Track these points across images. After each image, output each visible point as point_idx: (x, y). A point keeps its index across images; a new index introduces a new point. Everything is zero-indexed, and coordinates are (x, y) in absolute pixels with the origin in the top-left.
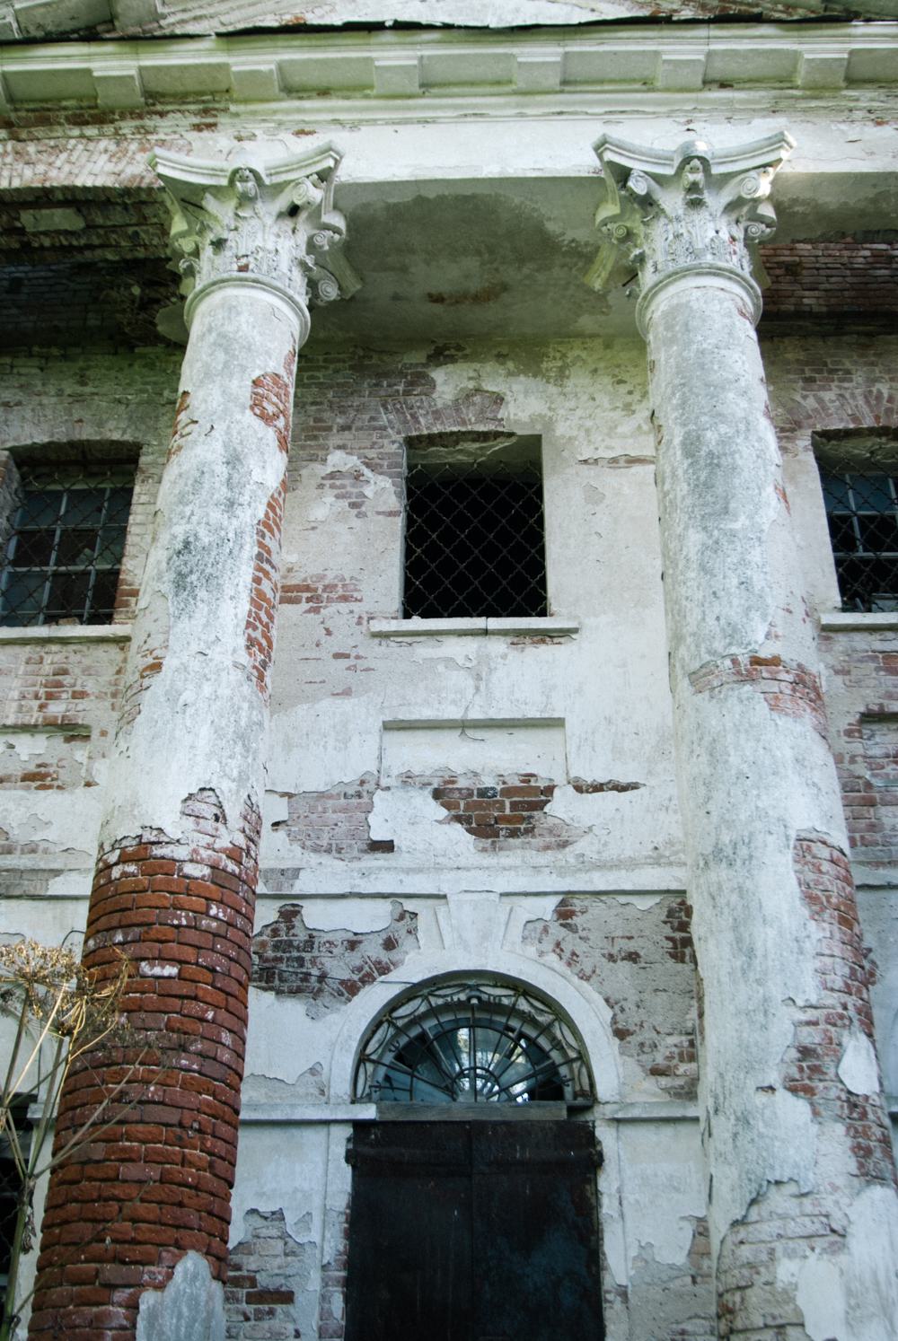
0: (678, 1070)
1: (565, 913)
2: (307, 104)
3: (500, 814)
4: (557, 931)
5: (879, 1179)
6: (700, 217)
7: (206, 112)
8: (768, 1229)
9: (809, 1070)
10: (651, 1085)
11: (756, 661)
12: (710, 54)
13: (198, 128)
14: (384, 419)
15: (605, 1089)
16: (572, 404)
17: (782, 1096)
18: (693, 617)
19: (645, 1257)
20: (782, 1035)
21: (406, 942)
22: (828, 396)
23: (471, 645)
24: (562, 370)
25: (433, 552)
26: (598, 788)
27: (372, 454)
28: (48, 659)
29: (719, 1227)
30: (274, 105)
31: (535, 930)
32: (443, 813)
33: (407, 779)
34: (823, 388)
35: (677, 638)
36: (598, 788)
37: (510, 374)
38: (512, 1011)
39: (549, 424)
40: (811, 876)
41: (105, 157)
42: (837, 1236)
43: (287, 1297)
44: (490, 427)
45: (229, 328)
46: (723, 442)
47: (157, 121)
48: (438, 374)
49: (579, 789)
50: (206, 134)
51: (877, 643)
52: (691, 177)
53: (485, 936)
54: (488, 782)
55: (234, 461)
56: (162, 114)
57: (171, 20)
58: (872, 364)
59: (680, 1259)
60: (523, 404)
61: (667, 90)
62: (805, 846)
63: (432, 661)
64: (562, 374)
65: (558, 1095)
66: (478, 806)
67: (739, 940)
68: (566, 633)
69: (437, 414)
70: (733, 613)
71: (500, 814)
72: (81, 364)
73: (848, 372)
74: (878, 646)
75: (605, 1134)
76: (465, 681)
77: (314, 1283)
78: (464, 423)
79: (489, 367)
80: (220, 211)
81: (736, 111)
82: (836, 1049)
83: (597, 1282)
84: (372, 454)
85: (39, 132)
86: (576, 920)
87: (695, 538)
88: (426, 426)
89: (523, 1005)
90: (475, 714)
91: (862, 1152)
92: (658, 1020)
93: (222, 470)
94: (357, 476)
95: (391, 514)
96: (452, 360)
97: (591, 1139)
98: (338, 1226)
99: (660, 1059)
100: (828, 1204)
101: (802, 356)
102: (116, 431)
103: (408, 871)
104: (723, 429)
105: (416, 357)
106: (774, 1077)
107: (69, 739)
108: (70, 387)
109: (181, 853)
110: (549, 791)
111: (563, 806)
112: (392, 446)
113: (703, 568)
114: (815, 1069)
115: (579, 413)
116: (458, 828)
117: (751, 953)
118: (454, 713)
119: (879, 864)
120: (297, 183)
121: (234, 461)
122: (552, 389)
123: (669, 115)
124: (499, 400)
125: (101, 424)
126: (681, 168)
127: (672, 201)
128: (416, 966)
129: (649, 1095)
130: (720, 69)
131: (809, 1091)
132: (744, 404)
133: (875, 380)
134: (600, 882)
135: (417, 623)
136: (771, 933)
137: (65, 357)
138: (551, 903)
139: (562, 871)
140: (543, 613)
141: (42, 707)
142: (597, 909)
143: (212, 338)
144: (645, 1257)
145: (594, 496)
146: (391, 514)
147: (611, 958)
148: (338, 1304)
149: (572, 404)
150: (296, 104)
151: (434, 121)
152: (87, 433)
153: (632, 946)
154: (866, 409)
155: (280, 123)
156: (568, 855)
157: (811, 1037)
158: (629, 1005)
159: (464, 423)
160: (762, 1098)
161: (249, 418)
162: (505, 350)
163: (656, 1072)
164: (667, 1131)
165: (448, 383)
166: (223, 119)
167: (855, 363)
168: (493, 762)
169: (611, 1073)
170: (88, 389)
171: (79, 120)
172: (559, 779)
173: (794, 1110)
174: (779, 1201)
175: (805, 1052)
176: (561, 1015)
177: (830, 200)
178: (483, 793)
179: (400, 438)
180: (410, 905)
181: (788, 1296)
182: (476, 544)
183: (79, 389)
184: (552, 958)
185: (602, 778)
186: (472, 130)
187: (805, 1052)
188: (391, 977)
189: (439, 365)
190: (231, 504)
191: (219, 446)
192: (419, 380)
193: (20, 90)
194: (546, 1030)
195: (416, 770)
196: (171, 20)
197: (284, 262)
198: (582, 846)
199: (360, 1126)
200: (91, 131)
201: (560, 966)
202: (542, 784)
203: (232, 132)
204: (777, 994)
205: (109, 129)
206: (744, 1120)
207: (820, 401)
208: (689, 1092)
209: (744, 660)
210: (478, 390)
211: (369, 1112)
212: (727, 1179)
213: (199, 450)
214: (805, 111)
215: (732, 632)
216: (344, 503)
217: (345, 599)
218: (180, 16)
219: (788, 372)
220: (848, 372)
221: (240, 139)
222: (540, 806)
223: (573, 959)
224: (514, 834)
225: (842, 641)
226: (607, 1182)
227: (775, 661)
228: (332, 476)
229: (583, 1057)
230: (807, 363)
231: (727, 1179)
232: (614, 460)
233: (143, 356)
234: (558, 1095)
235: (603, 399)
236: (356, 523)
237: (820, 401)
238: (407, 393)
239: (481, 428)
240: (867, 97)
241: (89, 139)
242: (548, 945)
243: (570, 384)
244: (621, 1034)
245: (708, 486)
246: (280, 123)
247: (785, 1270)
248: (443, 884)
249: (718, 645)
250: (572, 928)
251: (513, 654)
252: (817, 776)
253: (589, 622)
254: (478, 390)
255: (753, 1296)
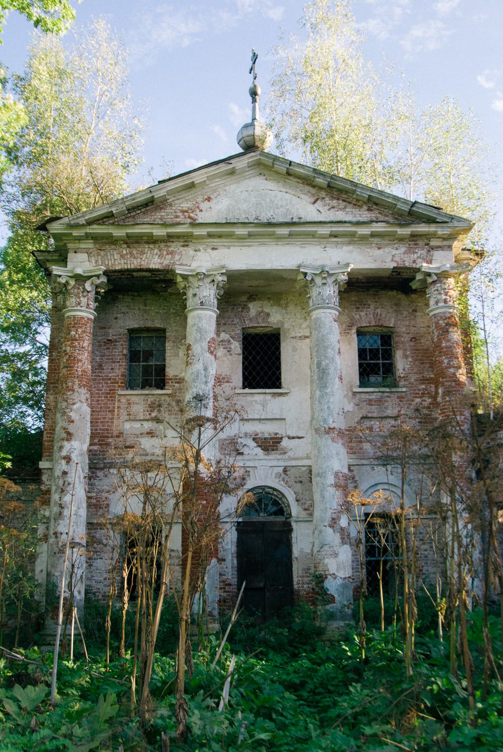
0: (309, 509)
1: (285, 471)
2: (215, 240)
3: (270, 444)
4: (283, 476)
5: (346, 543)
6: (326, 288)
7: (185, 241)
8: (323, 553)
9: (334, 522)
10: (304, 513)
11: (330, 428)
12: (331, 231)
13: (183, 246)
14: (236, 321)
15: (294, 513)
16: (289, 317)
17: (328, 527)
18: (316, 414)
19: (301, 551)
20: (328, 515)
21: (248, 478)
22: (362, 314)
23: (262, 397)
24: (287, 304)
25: (250, 373)
26: (294, 438)
27: (233, 333)
28: (149, 400)
29: (315, 552)
30: (205, 240)
31: (278, 476)
32: (255, 445)
33: (246, 435)
34: (361, 311)
35: (313, 419)
36: (294, 438)
37: (272, 305)
38: (273, 494)
39: (283, 324)
40: (337, 481)
41: (157, 256)
42: (336, 555)
43: (224, 560)
44: (266, 325)
45: (200, 325)
46: (327, 365)
47: (171, 244)
48: (251, 305)
49: (289, 438)
50: (185, 248)
51: (367, 396)
52: (324, 276)
53: (266, 477)
54: (266, 436)
55: (206, 369)
56: (173, 242)
57: (170, 200)
58: (377, 302)
59: (309, 551)
60: (276, 317)
61: (319, 238)
62: (336, 475)
63: (252, 401)
64: (287, 306)
65: (283, 515)
66: (264, 442)
67: (322, 494)
68: (286, 393)
69: (251, 320)
70: (325, 416)
71: (270, 444)
72: (144, 298)
73: (369, 305)
74: (367, 397)
75: (293, 524)
76: (259, 407)
77: (230, 557)
78: (258, 323)
79: (266, 302)
80: (194, 282)
81: (338, 244)
82: (339, 518)
83: (291, 556)
84: (233, 333)
85: (136, 245)
86: (288, 473)
87: (318, 393)
88: (248, 324)
89: (275, 493)
90: (262, 417)
91: (343, 538)
92: (306, 497)
93: (203, 372)
94: (229, 341)
95: (239, 354)
96: (254, 300)
97: (290, 525)
98: (235, 545)
99: (306, 506)
100: (335, 549)
101: (356, 299)
102: (158, 324)
103: (248, 460)
104: (327, 361)
105: (244, 298)
106: (326, 524)
107: (157, 423)
108: (142, 307)
109: (204, 475)
110: (281, 438)
111: (285, 443)
112: (239, 331)
113: (319, 402)
114: (335, 523)
115: (291, 320)
116: (259, 449)
117: (324, 497)
118: (257, 417)
119: (361, 459)
120: (215, 275)
121: (206, 369)
122: (284, 311)
123: (319, 245)
124: (268, 315)
125: (153, 321)
126: (321, 273)
127: (318, 281)
128: (250, 484)
129: (304, 515)
130: (333, 233)
131: (333, 527)
132: (332, 352)
133: (377, 308)
134: (294, 463)
135: (247, 390)
136: (328, 494)
137: (139, 296)
138: (282, 469)
139: (285, 460)
140: (280, 388)
141: (150, 414)
142: (293, 470)
143: (196, 327)
144: (301, 551)
145: (295, 349)
146: (239, 354)
147: (296, 482)
148: (235, 561)
149: (289, 317)
150: (212, 240)
151: (252, 246)
152: (149, 324)
153: (300, 479)
154: (373, 319)
155: (207, 245)
156: (286, 456)
157: (334, 516)
158: (300, 494)
159: (258, 323)
160: (324, 528)
161: (208, 355)
162: (270, 296)
163: (305, 509)
164: (308, 523)
165: (254, 308)
166: (190, 244)
167: (372, 301)
168: (267, 430)
169: (295, 510)
170: (148, 308)
171: (148, 243)
172: (284, 435)
173: (330, 530)
174: (326, 548)
175: (333, 519)
176: (284, 496)
177: (364, 272)
178: (265, 439)
179: (240, 328)
180: (248, 469)
181: (326, 565)
182: (262, 364)
183: (145, 308)
184: (282, 482)
185: (294, 435)
186: (262, 249)
187: (333, 519)
188: (244, 487)
189: (251, 302)
190: (206, 382)
191: (201, 364)
192: (245, 307)
193: (130, 235)
194: (280, 499)
195: (248, 432)
196: (170, 200)
197: (212, 297)
198: (290, 454)
199: (238, 523)
200: (152, 246)
201: (284, 484)
202: (280, 436)
203: (194, 248)
204: (328, 506)
205: (157, 246)
206: (320, 532)
207: (360, 316)
208: (311, 515)
209: (327, 428)
210: (262, 311)
211: (240, 520)
212: (317, 543)
213: (197, 366)
214: (359, 244)
215: (325, 421)
216: (226, 350)
217: (228, 382)
218: (173, 199)
219: (352, 305)
220: (369, 305)
221: (196, 251)
222: (279, 442)
223: (287, 483)
224: (273, 450)
225: (358, 396)
226: (294, 535)
227: (334, 428)
228: (222, 341)
229: (289, 506)
230: (358, 302)
231: (317, 543)
232: (301, 337)
233: (163, 296)
234: (283, 515)
235: (298, 316)
236: (230, 357)
237: (360, 316)
238: (242, 311)
239: (264, 325)
240: (376, 240)
241: (152, 249)
242: (281, 479)
243: (288, 309)
244: (297, 501)
245: (322, 378)
246: (207, 245)
247: (326, 561)
248: (256, 464)
249: (322, 424)
250: (287, 475)
251: (273, 399)
252: (341, 457)
253: (293, 390)
254: (262, 311)
255: (321, 565)
